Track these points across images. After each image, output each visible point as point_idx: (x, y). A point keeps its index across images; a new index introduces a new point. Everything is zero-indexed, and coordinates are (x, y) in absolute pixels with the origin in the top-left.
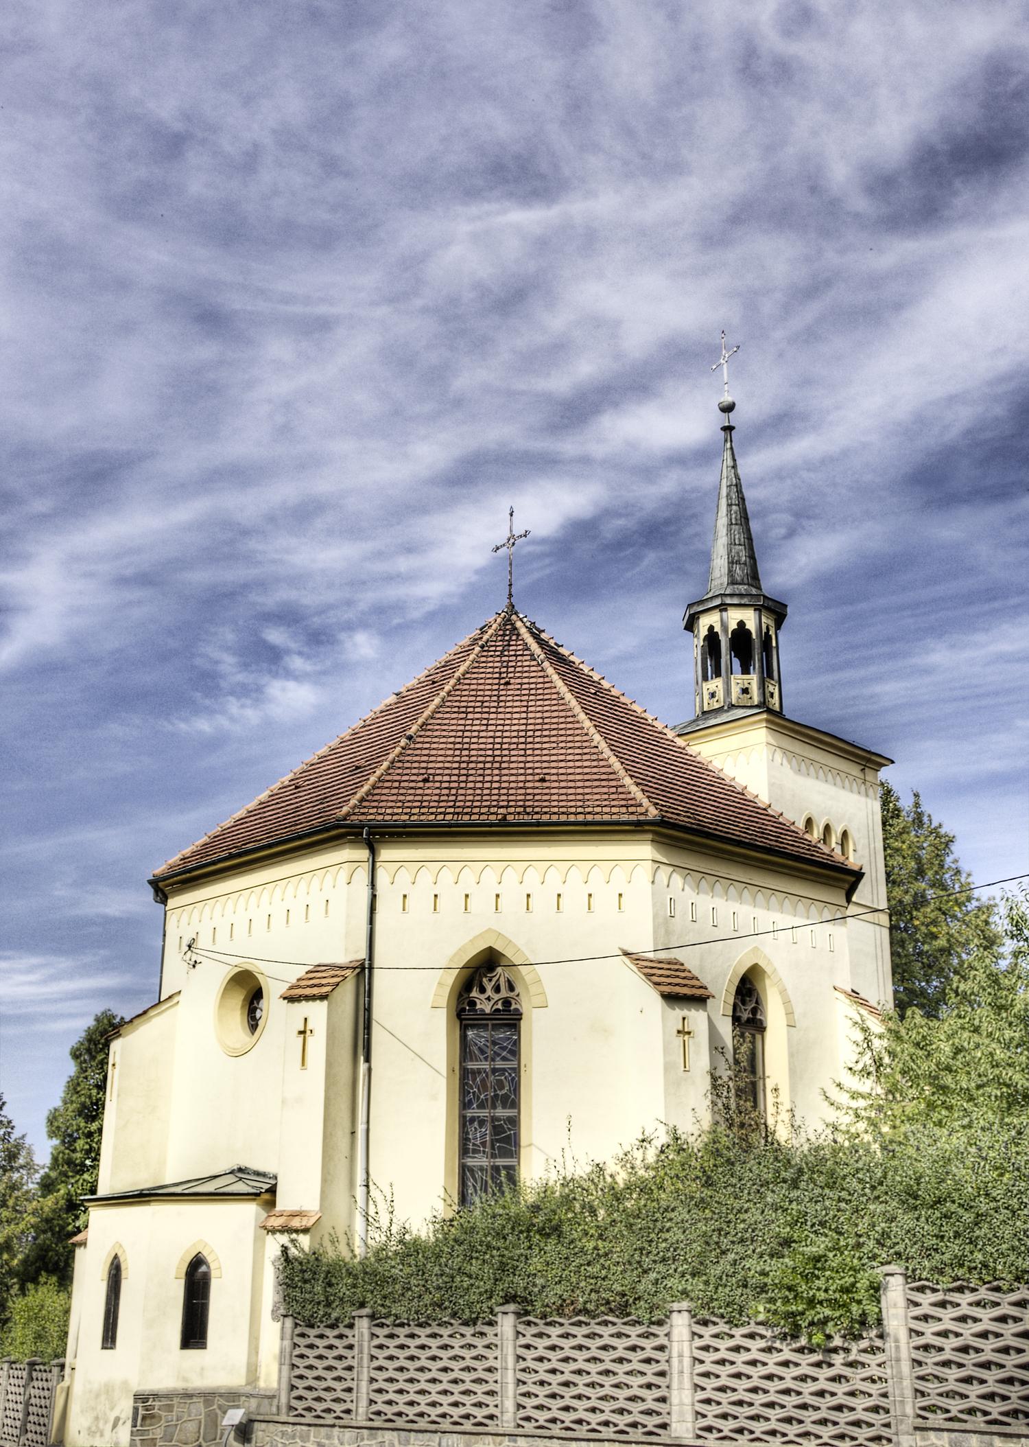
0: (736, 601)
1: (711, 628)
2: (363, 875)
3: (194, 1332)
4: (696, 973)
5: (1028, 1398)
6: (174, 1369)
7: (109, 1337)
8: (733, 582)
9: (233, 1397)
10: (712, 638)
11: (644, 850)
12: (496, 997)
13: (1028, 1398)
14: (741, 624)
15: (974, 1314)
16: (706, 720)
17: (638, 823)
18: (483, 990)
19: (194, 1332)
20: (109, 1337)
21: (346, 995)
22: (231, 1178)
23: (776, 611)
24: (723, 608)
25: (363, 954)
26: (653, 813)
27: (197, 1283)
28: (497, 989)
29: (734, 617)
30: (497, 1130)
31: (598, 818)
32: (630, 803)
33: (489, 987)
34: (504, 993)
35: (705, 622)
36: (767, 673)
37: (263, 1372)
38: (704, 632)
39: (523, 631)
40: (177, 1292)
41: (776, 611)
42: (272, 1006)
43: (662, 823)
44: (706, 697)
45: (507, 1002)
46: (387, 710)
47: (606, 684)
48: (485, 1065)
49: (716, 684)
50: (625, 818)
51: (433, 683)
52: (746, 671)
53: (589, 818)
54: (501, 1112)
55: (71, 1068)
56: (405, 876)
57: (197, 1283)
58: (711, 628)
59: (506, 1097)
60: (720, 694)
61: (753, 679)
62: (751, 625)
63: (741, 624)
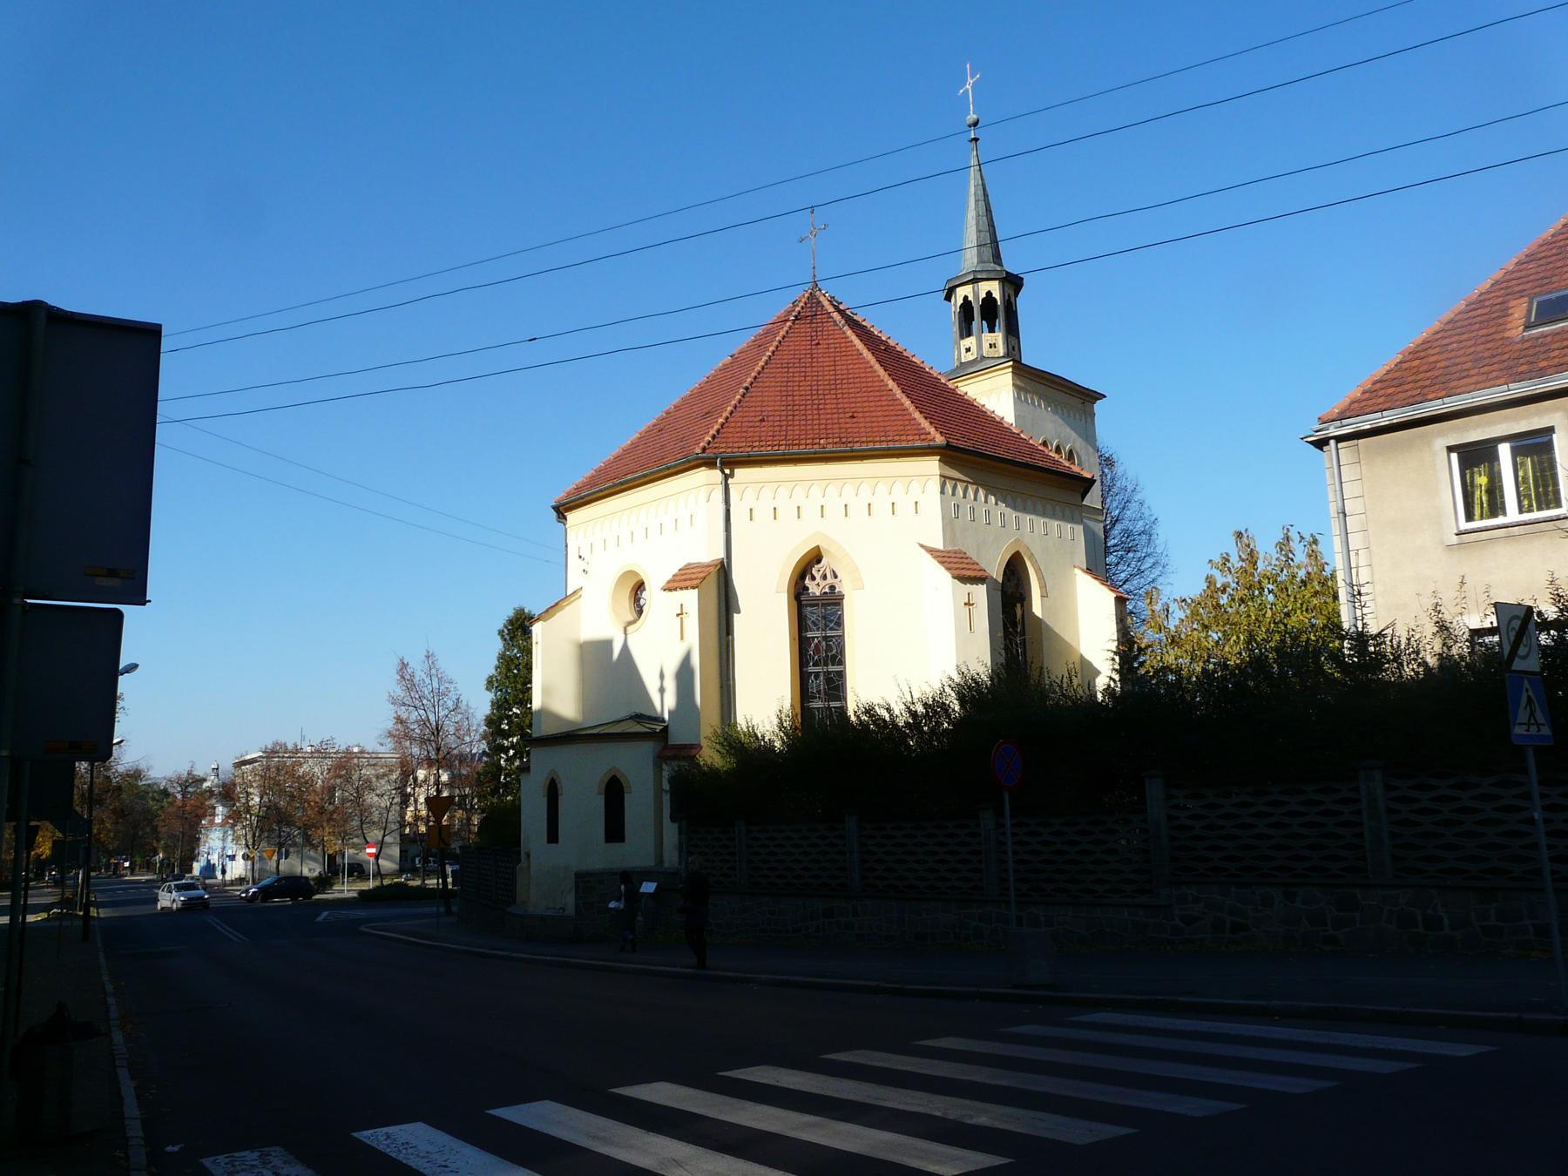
0: (984, 276)
1: (966, 298)
2: (719, 494)
3: (615, 830)
4: (975, 559)
5: (1566, 821)
6: (604, 857)
7: (553, 837)
8: (981, 261)
9: (647, 875)
10: (966, 305)
11: (932, 465)
12: (823, 583)
13: (1566, 821)
14: (989, 293)
15: (456, 867)
16: (966, 370)
17: (929, 447)
18: (813, 578)
19: (615, 830)
20: (553, 837)
21: (712, 585)
22: (631, 723)
23: (1013, 283)
24: (975, 281)
25: (721, 554)
26: (940, 440)
27: (614, 791)
28: (824, 577)
29: (983, 288)
30: (829, 680)
31: (897, 445)
32: (921, 433)
33: (818, 576)
34: (830, 580)
35: (961, 292)
36: (1012, 330)
37: (666, 855)
38: (960, 301)
39: (826, 303)
40: (597, 804)
41: (1013, 283)
42: (652, 596)
43: (948, 446)
44: (963, 351)
45: (832, 588)
46: (725, 368)
47: (891, 342)
48: (818, 634)
49: (970, 342)
50: (918, 444)
51: (759, 345)
52: (992, 330)
53: (891, 445)
54: (831, 668)
55: (498, 645)
56: (750, 493)
57: (614, 791)
58: (966, 298)
59: (834, 657)
60: (974, 349)
61: (998, 337)
62: (997, 295)
63: (989, 293)
